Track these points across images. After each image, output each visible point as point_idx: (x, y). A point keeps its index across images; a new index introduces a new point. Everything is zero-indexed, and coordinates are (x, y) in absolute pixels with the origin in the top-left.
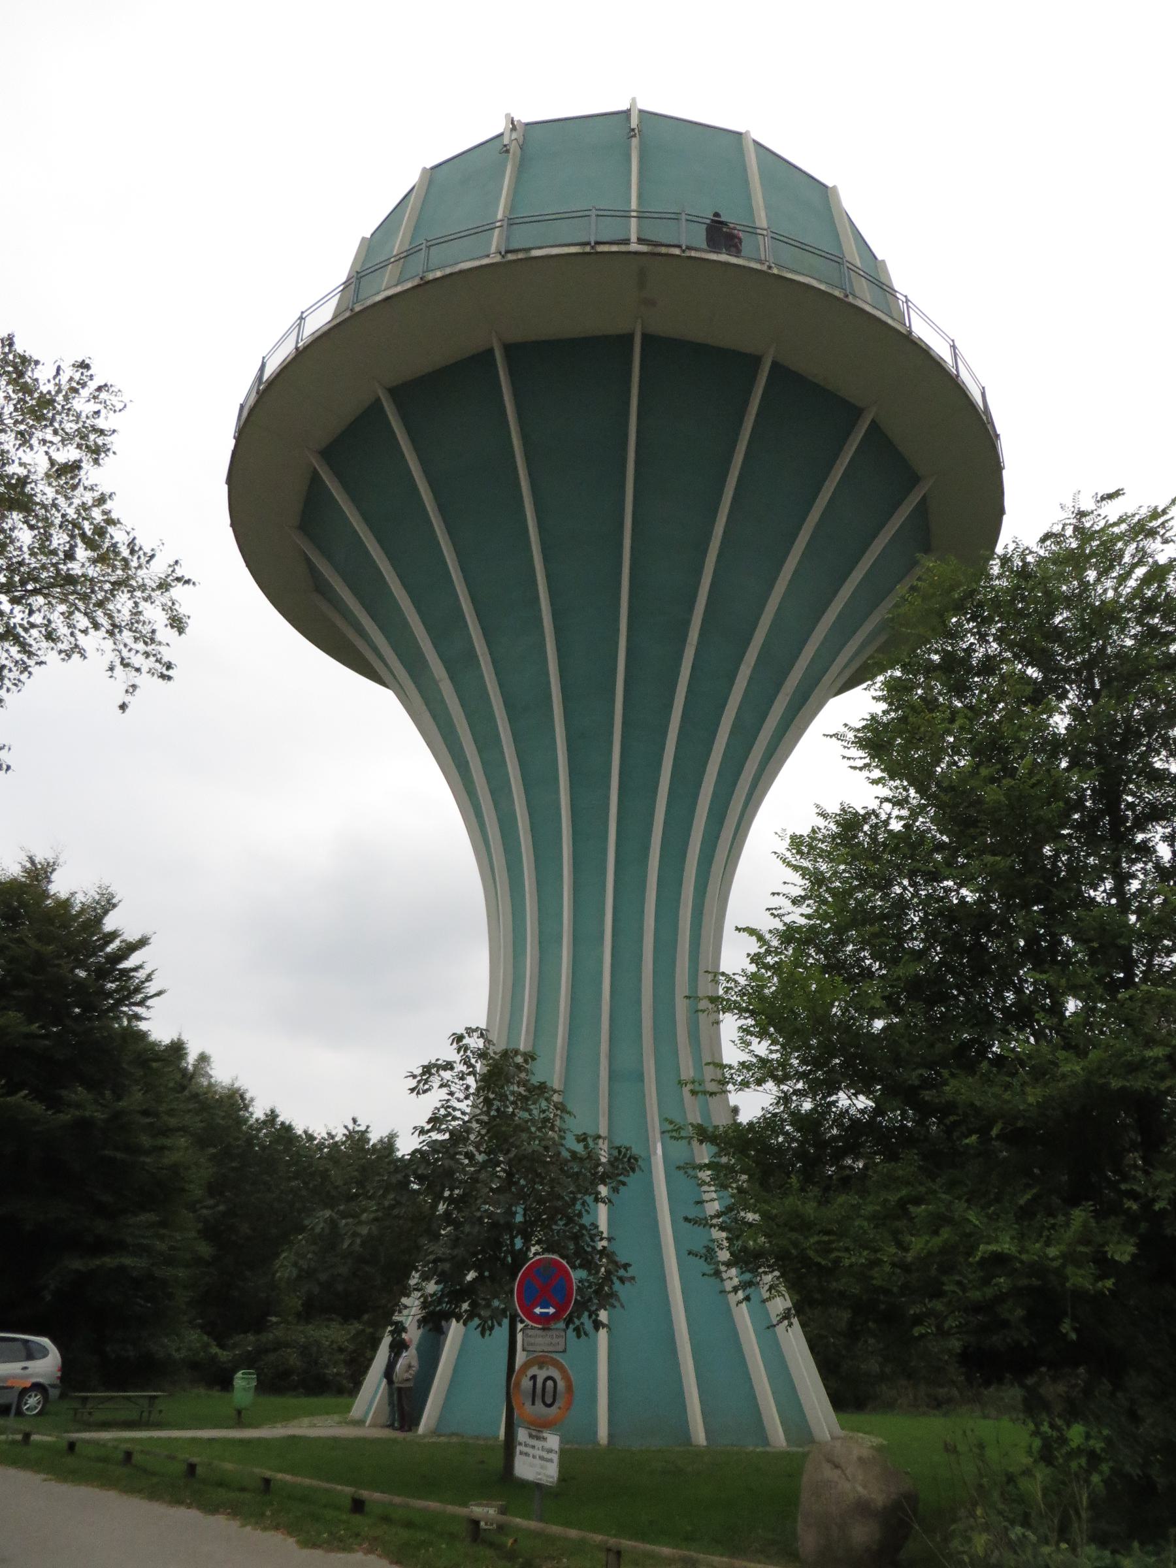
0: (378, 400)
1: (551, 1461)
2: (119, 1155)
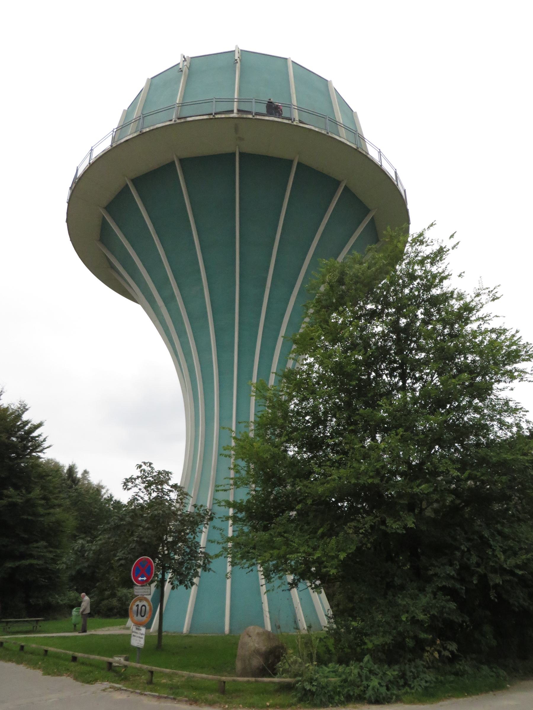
0: (127, 185)
1: (142, 638)
2: (30, 518)
